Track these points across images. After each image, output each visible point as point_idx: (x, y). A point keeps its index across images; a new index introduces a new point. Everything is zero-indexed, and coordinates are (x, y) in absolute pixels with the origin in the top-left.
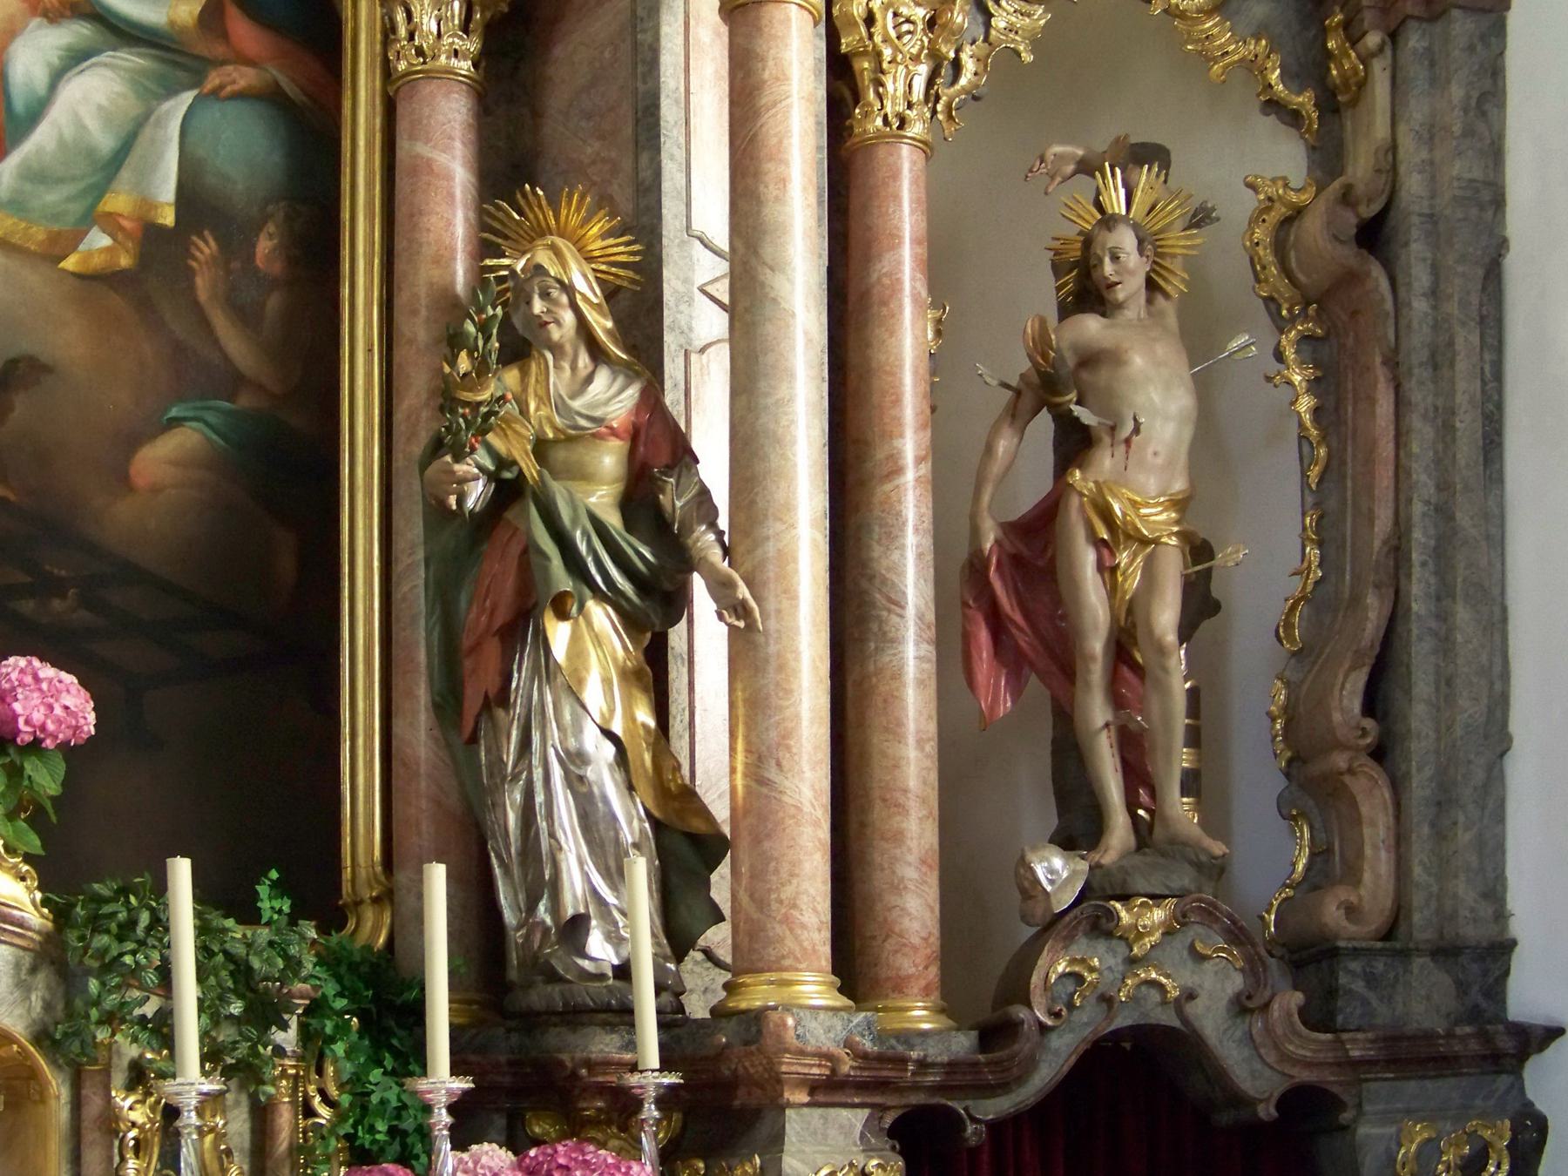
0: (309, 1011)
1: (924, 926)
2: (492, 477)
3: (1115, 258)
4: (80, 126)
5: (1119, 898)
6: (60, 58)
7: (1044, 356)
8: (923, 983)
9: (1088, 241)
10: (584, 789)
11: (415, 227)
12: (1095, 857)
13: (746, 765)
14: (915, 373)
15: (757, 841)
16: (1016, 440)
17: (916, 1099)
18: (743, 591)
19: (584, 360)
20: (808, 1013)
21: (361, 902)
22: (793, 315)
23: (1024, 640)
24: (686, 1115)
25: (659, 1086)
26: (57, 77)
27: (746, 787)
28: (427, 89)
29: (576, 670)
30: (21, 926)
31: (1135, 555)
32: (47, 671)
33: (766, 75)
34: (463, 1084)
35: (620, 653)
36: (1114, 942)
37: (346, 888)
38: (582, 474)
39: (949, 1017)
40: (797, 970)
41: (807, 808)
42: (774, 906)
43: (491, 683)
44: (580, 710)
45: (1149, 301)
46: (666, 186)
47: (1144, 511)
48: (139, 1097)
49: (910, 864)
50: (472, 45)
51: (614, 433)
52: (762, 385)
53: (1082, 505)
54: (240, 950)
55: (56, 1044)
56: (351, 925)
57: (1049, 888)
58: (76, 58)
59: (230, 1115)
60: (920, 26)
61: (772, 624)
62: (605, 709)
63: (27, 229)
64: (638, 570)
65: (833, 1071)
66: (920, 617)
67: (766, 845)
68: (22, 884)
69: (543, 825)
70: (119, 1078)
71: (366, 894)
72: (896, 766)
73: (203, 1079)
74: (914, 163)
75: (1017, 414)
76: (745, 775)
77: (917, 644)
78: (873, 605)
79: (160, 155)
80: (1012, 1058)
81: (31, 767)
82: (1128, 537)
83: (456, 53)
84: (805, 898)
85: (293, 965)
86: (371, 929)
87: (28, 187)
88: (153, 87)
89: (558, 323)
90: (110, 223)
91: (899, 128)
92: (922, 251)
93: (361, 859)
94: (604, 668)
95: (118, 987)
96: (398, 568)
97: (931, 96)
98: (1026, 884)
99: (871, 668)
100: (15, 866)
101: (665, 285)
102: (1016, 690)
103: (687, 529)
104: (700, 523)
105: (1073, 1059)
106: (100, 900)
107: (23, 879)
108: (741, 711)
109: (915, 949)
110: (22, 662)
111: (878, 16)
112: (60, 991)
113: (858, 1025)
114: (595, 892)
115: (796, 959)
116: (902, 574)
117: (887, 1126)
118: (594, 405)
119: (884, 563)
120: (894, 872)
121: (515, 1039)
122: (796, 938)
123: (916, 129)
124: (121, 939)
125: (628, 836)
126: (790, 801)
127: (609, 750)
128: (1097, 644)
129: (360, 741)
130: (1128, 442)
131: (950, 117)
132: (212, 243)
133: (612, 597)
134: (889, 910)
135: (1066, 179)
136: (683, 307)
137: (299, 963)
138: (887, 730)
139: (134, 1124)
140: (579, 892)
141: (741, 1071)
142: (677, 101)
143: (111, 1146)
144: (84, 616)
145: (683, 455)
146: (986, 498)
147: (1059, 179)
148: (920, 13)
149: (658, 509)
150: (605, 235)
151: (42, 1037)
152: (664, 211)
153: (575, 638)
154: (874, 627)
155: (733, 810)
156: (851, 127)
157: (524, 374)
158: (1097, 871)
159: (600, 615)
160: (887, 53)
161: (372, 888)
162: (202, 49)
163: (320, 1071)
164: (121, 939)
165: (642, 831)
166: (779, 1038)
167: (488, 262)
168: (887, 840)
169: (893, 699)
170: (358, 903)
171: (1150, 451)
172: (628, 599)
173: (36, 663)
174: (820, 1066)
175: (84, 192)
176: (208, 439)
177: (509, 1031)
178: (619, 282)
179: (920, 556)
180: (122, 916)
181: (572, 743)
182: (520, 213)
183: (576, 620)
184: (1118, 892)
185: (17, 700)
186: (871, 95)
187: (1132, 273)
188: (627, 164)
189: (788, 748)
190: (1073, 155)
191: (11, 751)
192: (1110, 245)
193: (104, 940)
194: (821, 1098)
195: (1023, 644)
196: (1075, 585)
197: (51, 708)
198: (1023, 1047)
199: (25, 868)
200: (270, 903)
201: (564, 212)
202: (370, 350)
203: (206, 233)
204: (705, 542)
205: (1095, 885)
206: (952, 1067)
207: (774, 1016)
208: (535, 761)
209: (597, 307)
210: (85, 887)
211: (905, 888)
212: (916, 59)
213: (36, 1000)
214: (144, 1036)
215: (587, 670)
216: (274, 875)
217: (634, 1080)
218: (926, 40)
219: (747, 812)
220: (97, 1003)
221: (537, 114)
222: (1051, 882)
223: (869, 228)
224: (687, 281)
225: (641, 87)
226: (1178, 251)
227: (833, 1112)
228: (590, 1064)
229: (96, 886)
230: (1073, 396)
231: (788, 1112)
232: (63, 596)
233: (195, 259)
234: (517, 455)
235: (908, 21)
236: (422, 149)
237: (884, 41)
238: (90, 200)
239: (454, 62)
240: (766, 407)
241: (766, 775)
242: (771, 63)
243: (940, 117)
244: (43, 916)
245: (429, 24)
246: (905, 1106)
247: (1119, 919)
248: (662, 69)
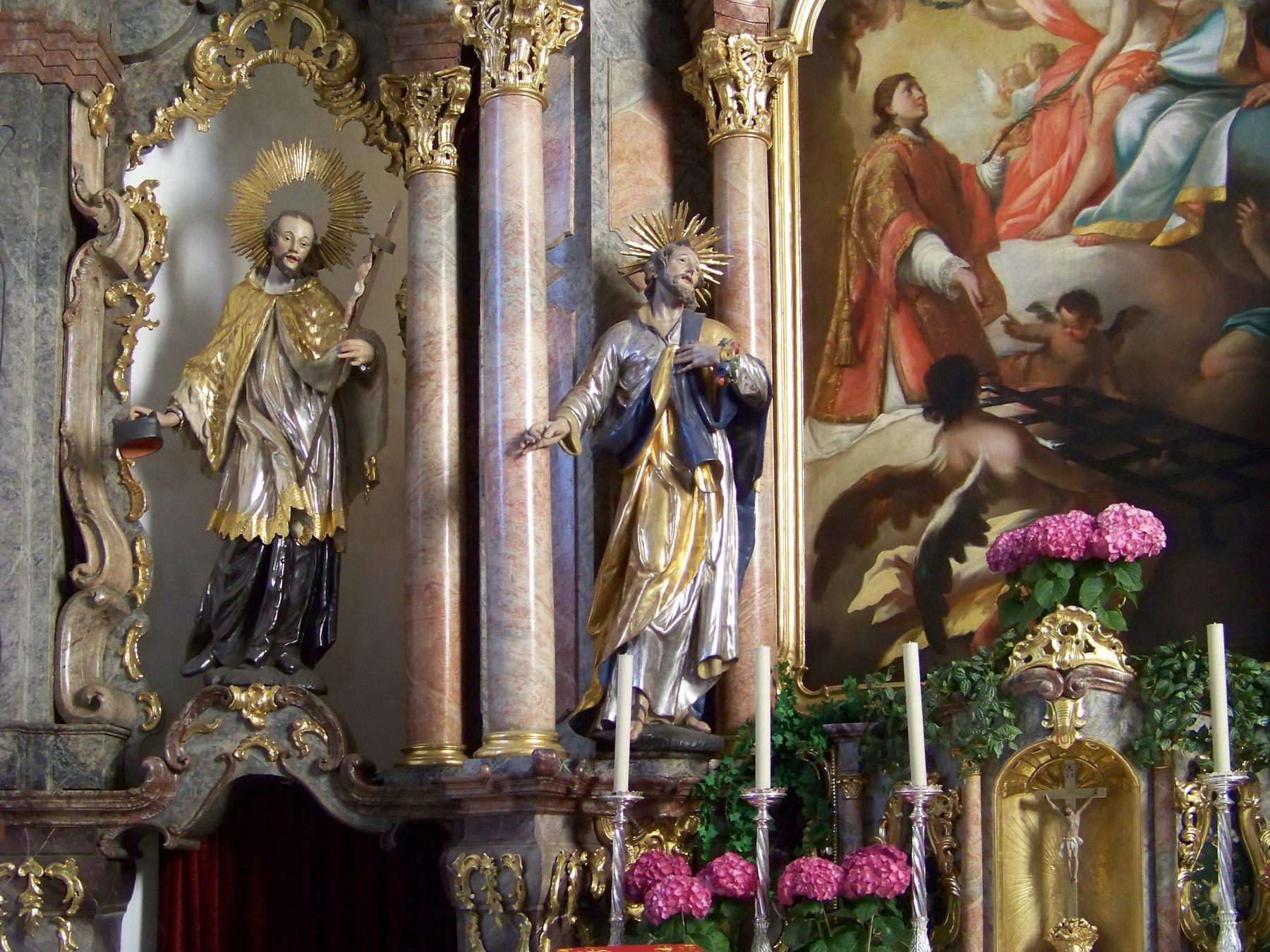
4: (1162, 153)
6: (1149, 113)
26: (1146, 126)
32: (1132, 511)
48: (1196, 786)
55: (1135, 753)
58: (1158, 111)
59: (1263, 795)
63: (1130, 226)
70: (1181, 773)
73: (1231, 773)
81: (1120, 576)
87: (1131, 199)
88: (1209, 114)
90: (1183, 210)
95: (1175, 713)
100: (1109, 640)
106: (1164, 657)
107: (1114, 648)
110: (1116, 507)
124: (1176, 681)
132: (1253, 204)
139: (1192, 804)
143: (1174, 820)
151: (1127, 749)
164: (1176, 681)
173: (1126, 506)
175: (1167, 193)
180: (1177, 666)
185: (1108, 533)
191: (1107, 567)
193: (1165, 683)
197: (1130, 535)
199: (1115, 641)
203: (1249, 199)
210: (1156, 648)
213: (1124, 726)
214: (1192, 745)
220: (1161, 725)
229: (1162, 648)
232: (1158, 456)
233: (1241, 218)
238: (1170, 197)
244: (1127, 671)
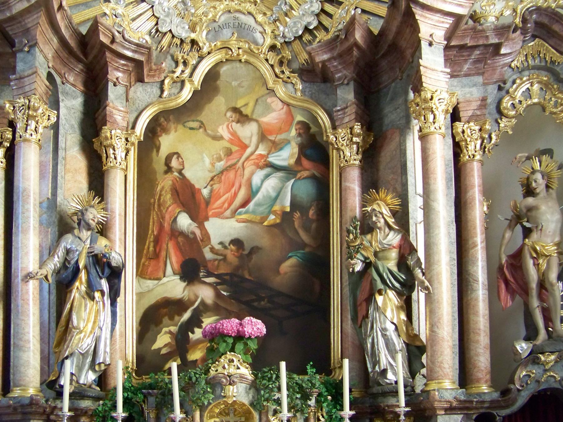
0: (318, 396)
1: (485, 364)
2: (363, 262)
3: (536, 182)
4: (268, 191)
5: (541, 353)
7: (516, 210)
8: (485, 379)
9: (528, 179)
10: (386, 337)
11: (346, 203)
12: (535, 342)
13: (429, 328)
14: (480, 220)
15: (432, 347)
16: (511, 233)
17: (482, 411)
18: (427, 283)
19: (387, 230)
20: (444, 390)
21: (336, 368)
22: (439, 212)
23: (514, 286)
24: (414, 418)
25: (404, 411)
27: (429, 333)
28: (348, 169)
29: (384, 308)
30: (247, 379)
31: (544, 260)
32: (254, 320)
33: (430, 153)
34: (353, 413)
35: (396, 303)
36: (540, 365)
37: (332, 365)
38: (386, 259)
39: (493, 388)
40: (442, 379)
41: (445, 337)
42: (436, 363)
43: (364, 313)
44: (385, 317)
45: (547, 191)
46: (409, 183)
47: (546, 248)
49: (481, 348)
50: (360, 157)
51: (394, 247)
52: (431, 231)
53: (528, 248)
54: (300, 382)
56: (333, 374)
57: (521, 352)
58: (267, 176)
60: (477, 131)
61: (436, 291)
62: (392, 317)
64: (401, 281)
65: (451, 405)
66: (483, 283)
67: (434, 347)
68: (247, 369)
69: (376, 347)
71: (337, 366)
72: (477, 323)
74: (477, 166)
75: (511, 226)
76: (429, 330)
77: (482, 290)
78: (470, 282)
79: (286, 196)
80: (509, 398)
82: (542, 255)
83: (355, 160)
84: (445, 361)
85: (313, 385)
86: (336, 375)
87: (256, 208)
89: (379, 222)
90: (275, 213)
91: (473, 158)
92: (481, 188)
93: (336, 358)
94: (391, 306)
96: (343, 286)
97: (483, 148)
98: (515, 351)
99: (469, 298)
100: (245, 365)
101: (410, 208)
102: (513, 299)
103: (414, 269)
104: (417, 267)
105: (528, 398)
106: (265, 372)
107: (247, 368)
108: (428, 313)
109: (482, 371)
111: (465, 131)
112: (256, 394)
113: (460, 393)
114: (389, 363)
115: (442, 377)
116: (477, 273)
117: (474, 418)
118: (389, 241)
119: (472, 270)
120: (476, 351)
121: (371, 400)
122: (442, 371)
123: (478, 157)
124: (269, 381)
125: (398, 348)
126: (441, 336)
127: (394, 327)
128: (534, 285)
129: (336, 329)
130: (541, 230)
131: (489, 152)
132: (299, 213)
133: (394, 288)
134: (475, 361)
135: (523, 162)
136: (415, 213)
137: (315, 384)
138: (474, 314)
140: (385, 363)
141: (426, 406)
142: (412, 162)
144: (268, 305)
145: (413, 250)
146: (503, 249)
147: (521, 163)
148: (477, 128)
149: (407, 264)
150: (391, 199)
151: (252, 404)
152: (409, 190)
153: (384, 300)
154: (470, 287)
155: (426, 339)
156: (460, 160)
157: (372, 235)
158: (535, 346)
159: (391, 294)
160: (469, 139)
161: (338, 364)
162: (296, 169)
163: (322, 410)
164: (269, 381)
165: (402, 346)
166: (433, 398)
167: (363, 209)
168: (474, 343)
169: (476, 306)
170: (335, 368)
171: (548, 232)
172: (398, 289)
173: (252, 318)
174: (447, 404)
175: (269, 206)
176: (298, 260)
177: (370, 398)
178: (398, 210)
179: (482, 267)
180: (269, 376)
181: (383, 326)
182: (370, 196)
183: (384, 295)
184: (541, 351)
186: (465, 151)
187: (541, 185)
188: (399, 179)
189: (440, 322)
190: (524, 156)
191: (245, 339)
192: (534, 178)
193: (264, 382)
194: (448, 412)
195: (514, 287)
196: (527, 270)
197: (253, 329)
198: (512, 396)
199: (248, 366)
200: (309, 370)
201: (380, 194)
202: (338, 234)
204: (418, 273)
205: (534, 350)
206: (492, 402)
207: (432, 392)
208: (375, 331)
209: (390, 217)
211: (480, 355)
212: (477, 139)
214: (274, 403)
215: (387, 308)
216: (311, 363)
217: (397, 410)
218: (479, 134)
219: (429, 340)
220: (263, 396)
221: (378, 170)
222: (521, 350)
223: (466, 185)
224: (415, 206)
225: (403, 160)
226: (555, 176)
227: (452, 416)
228: (388, 406)
230: (526, 220)
231: (438, 416)
232: (264, 300)
233: (295, 218)
234: (370, 256)
235: (474, 130)
236: (348, 184)
237: (468, 137)
238: (270, 208)
239: (355, 162)
240: (433, 236)
241: (434, 330)
242: (431, 150)
243: (486, 152)
245: (348, 154)
246: (478, 413)
247: (541, 359)
248: (407, 155)
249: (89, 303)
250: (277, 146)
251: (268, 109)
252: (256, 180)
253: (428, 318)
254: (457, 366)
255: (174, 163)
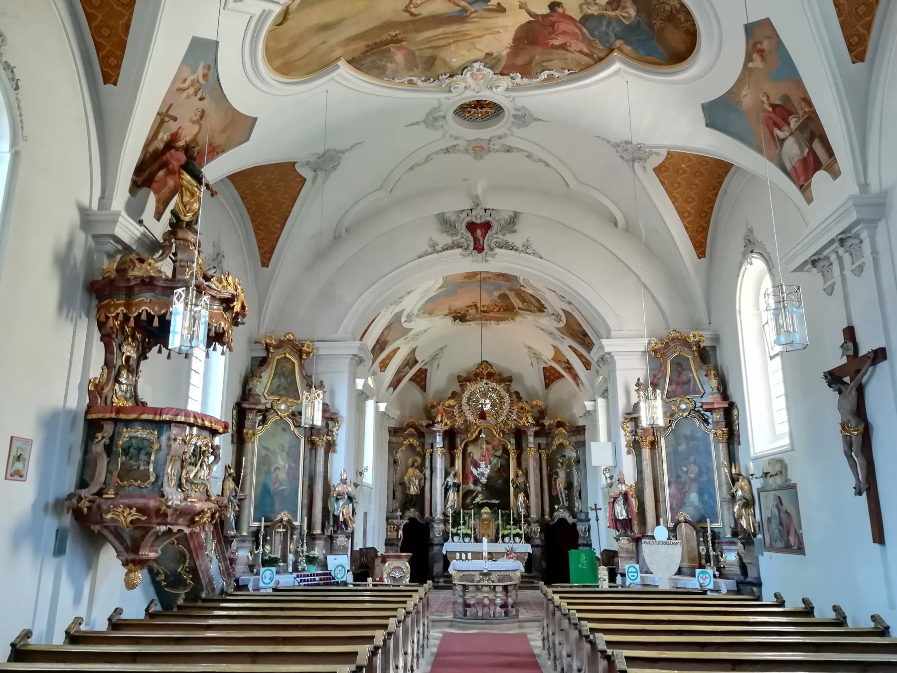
249: (138, 407)
250: (497, 451)
251: (494, 441)
252: (492, 459)
253: (561, 285)
254: (856, 405)
255: (471, 455)
